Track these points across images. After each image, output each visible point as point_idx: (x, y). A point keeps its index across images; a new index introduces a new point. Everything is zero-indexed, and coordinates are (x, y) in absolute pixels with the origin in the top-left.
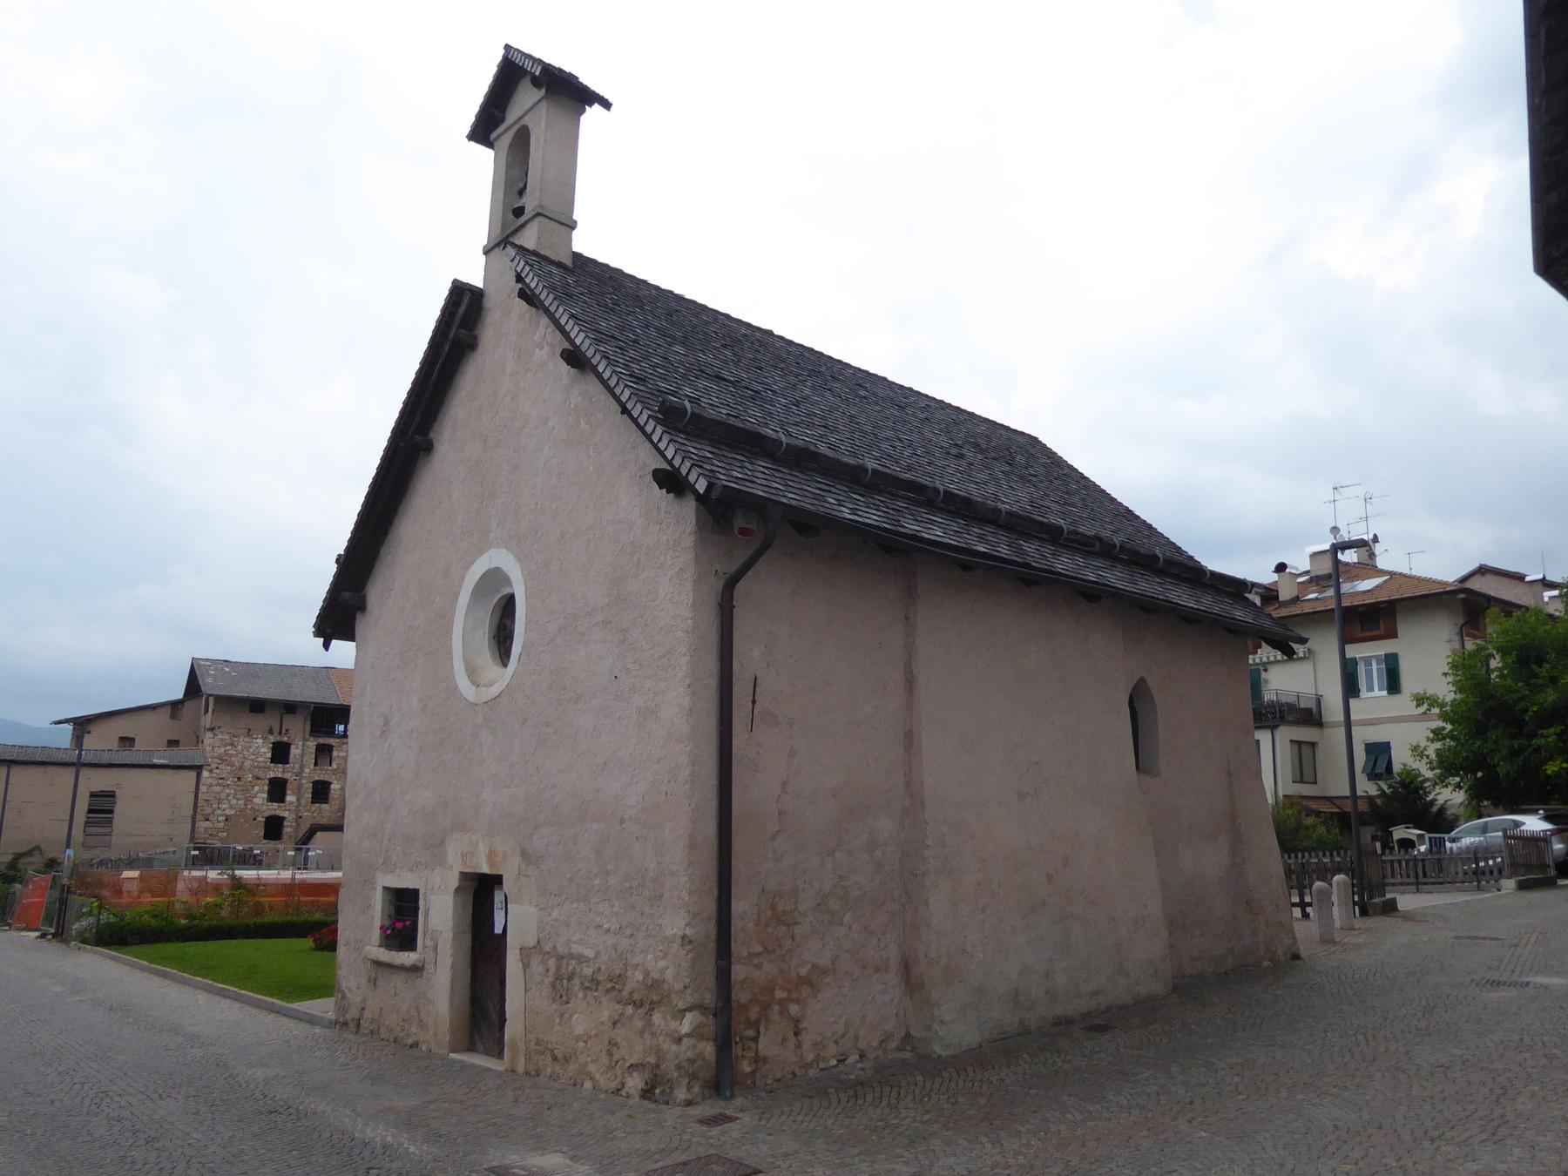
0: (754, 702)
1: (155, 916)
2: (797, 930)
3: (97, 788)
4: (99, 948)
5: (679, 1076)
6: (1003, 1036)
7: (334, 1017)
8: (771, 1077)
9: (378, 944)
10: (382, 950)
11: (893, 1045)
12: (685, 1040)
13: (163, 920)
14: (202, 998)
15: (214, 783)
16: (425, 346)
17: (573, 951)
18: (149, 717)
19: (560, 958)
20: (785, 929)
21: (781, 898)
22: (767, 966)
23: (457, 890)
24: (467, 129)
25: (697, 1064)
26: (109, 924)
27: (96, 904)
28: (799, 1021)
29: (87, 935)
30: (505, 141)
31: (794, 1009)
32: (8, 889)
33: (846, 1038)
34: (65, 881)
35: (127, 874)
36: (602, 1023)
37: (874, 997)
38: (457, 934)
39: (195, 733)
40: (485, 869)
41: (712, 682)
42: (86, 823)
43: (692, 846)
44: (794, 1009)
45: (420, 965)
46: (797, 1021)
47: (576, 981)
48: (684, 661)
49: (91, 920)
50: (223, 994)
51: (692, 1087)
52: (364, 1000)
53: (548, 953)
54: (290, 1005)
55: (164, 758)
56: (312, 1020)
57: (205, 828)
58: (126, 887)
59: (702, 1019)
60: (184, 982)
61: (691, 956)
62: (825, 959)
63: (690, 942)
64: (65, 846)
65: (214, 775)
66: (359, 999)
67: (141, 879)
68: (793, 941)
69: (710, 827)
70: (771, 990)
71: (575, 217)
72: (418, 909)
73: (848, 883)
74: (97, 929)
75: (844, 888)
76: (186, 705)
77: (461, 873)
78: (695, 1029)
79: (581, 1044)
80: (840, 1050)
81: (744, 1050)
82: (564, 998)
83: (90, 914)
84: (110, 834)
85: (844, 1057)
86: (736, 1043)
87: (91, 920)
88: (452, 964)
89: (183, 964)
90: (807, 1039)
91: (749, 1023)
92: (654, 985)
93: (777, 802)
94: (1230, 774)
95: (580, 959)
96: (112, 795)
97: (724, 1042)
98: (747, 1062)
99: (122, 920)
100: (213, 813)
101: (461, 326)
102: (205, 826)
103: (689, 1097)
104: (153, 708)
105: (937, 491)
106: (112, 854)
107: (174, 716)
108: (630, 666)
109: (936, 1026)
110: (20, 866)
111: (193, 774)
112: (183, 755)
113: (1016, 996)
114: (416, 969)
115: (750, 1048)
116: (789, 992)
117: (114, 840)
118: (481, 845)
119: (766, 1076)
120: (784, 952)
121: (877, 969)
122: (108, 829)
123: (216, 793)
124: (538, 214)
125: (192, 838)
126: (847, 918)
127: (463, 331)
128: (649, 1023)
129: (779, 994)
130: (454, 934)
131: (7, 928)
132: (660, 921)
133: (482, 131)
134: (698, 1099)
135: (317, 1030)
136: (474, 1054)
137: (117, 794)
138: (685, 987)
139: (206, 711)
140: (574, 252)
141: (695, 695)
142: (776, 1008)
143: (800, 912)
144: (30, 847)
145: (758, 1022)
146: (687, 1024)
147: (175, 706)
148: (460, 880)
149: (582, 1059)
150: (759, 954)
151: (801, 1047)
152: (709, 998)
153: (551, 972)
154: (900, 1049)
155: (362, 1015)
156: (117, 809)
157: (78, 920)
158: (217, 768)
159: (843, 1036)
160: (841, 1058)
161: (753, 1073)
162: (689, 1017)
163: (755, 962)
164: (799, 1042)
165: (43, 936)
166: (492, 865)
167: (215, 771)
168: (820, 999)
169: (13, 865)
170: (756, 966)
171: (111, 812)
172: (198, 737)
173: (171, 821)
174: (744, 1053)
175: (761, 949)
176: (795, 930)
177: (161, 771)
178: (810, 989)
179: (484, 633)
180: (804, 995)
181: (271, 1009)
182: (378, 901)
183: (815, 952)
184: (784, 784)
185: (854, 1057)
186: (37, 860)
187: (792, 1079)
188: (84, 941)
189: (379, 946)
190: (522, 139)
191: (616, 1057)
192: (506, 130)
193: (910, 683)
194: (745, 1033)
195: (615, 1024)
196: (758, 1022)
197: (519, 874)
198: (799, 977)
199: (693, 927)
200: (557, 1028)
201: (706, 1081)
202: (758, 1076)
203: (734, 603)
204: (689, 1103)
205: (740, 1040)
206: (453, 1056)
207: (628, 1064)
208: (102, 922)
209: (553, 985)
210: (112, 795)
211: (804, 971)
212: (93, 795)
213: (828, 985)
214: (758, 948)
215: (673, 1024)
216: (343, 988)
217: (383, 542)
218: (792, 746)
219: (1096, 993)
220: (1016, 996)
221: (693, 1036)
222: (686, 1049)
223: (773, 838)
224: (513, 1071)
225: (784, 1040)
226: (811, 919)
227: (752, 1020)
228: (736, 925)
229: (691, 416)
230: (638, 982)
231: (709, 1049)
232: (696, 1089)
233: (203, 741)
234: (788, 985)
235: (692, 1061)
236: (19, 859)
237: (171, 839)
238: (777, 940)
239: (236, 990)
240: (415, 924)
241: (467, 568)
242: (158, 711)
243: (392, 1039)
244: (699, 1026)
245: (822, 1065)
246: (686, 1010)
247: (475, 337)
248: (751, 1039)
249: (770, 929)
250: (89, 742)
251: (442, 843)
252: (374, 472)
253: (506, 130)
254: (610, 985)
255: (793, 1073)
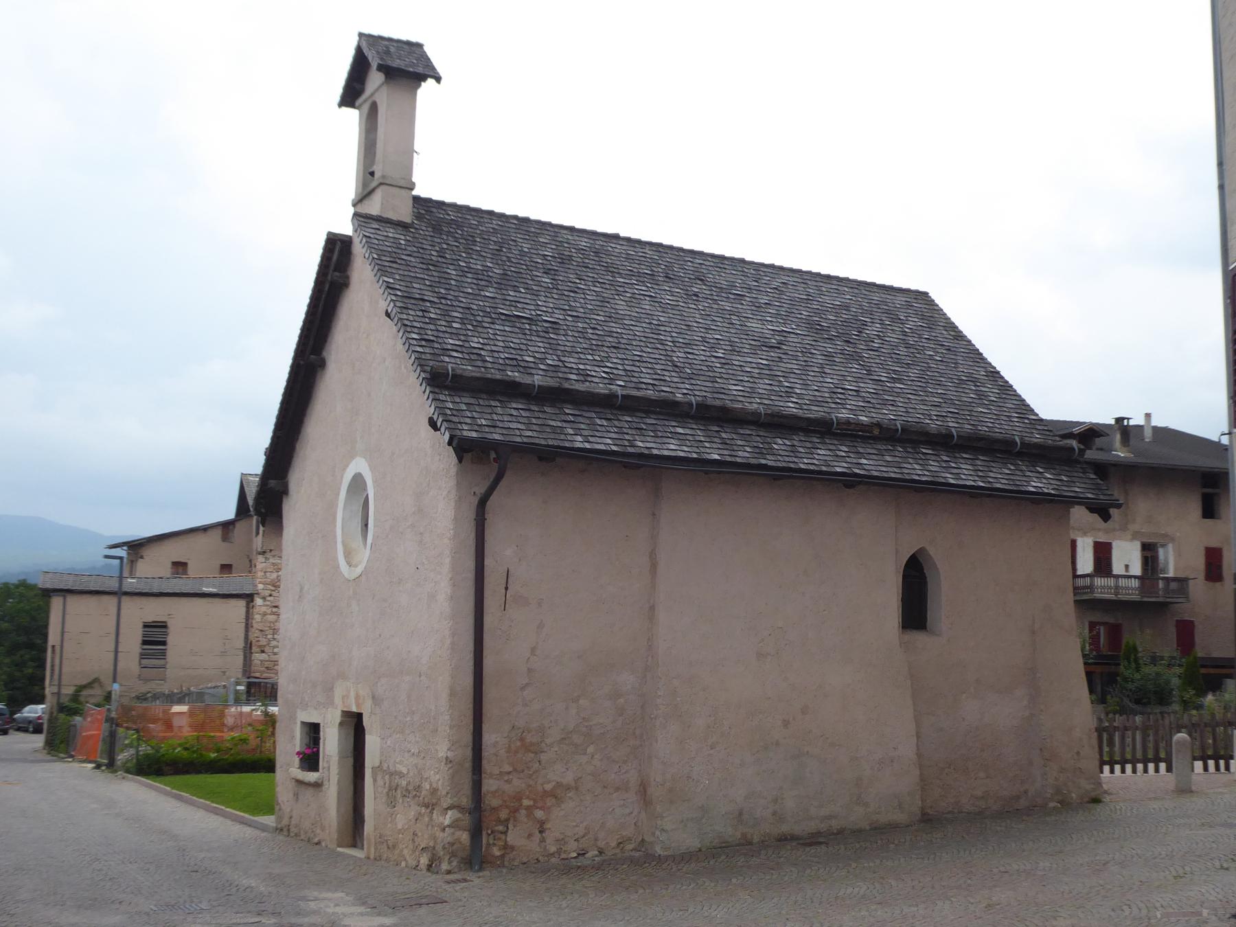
0: (506, 588)
1: (186, 749)
2: (543, 757)
3: (150, 618)
4: (139, 778)
5: (444, 855)
6: (724, 845)
7: (274, 825)
8: (518, 860)
9: (297, 767)
10: (299, 770)
11: (631, 847)
12: (447, 829)
13: (194, 752)
14: (200, 814)
15: (269, 611)
16: (312, 284)
17: (397, 769)
18: (201, 539)
19: (391, 774)
20: (532, 755)
21: (529, 732)
22: (516, 782)
23: (341, 724)
24: (338, 99)
25: (455, 847)
26: (147, 756)
27: (135, 736)
28: (544, 823)
29: (129, 765)
30: (366, 107)
31: (539, 814)
32: (70, 721)
33: (586, 838)
34: (113, 715)
35: (177, 709)
36: (410, 820)
37: (614, 809)
38: (342, 757)
39: (248, 556)
40: (354, 709)
41: (470, 575)
42: (141, 654)
43: (453, 694)
44: (539, 814)
45: (320, 781)
46: (542, 823)
47: (399, 792)
48: (448, 560)
49: (132, 751)
50: (216, 812)
51: (452, 862)
52: (291, 811)
53: (385, 771)
54: (256, 818)
55: (214, 586)
56: (263, 828)
57: (261, 661)
58: (176, 722)
59: (460, 815)
60: (192, 804)
61: (451, 771)
62: (569, 778)
63: (451, 761)
64: (111, 680)
65: (268, 603)
66: (288, 810)
67: (191, 713)
68: (540, 764)
69: (468, 681)
70: (520, 800)
71: (414, 180)
72: (320, 739)
73: (591, 723)
74: (138, 760)
75: (587, 727)
76: (238, 525)
77: (343, 711)
78: (453, 822)
79: (401, 836)
80: (581, 846)
81: (495, 840)
82: (393, 804)
83: (130, 746)
84: (164, 667)
85: (583, 852)
86: (489, 835)
87: (132, 751)
88: (338, 780)
89: (212, 795)
90: (550, 837)
91: (499, 821)
92: (434, 791)
93: (527, 662)
94: (1033, 632)
95: (401, 775)
96: (163, 626)
97: (476, 832)
98: (498, 848)
99: (158, 751)
100: (268, 644)
101: (335, 270)
102: (261, 658)
103: (449, 868)
104: (205, 529)
105: (690, 404)
106: (165, 688)
107: (225, 538)
108: (424, 561)
109: (658, 833)
110: (82, 699)
111: (242, 604)
112: (234, 583)
113: (741, 814)
114: (317, 785)
115: (500, 839)
116: (535, 801)
117: (169, 672)
118: (352, 690)
119: (514, 860)
120: (531, 773)
121: (617, 789)
122: (162, 662)
123: (271, 622)
124: (381, 184)
125: (81, 688)
126: (591, 749)
127: (337, 274)
128: (431, 819)
129: (526, 802)
130: (340, 757)
131: (70, 760)
132: (436, 747)
133: (350, 96)
134: (456, 870)
135: (264, 834)
136: (355, 849)
137: (169, 624)
138: (447, 793)
139: (258, 533)
140: (417, 199)
141: (454, 586)
142: (523, 812)
143: (546, 744)
144: (89, 680)
145: (507, 820)
146: (448, 819)
147: (226, 526)
148: (342, 716)
149: (401, 846)
150: (509, 773)
151: (545, 842)
152: (465, 801)
153: (387, 785)
154: (634, 849)
155: (290, 822)
156: (170, 640)
157: (122, 751)
158: (271, 595)
159: (584, 836)
160: (581, 852)
161: (503, 856)
162: (450, 813)
163: (506, 778)
164: (544, 838)
165: (98, 767)
166: (358, 705)
167: (269, 598)
168: (563, 807)
169: (75, 697)
170: (506, 781)
171: (164, 643)
172: (250, 561)
173: (223, 654)
174: (495, 842)
175: (511, 769)
176: (542, 757)
177: (210, 600)
178: (554, 800)
179: (358, 523)
180: (549, 804)
181: (243, 822)
182: (298, 731)
183: (557, 774)
184: (533, 650)
185: (592, 853)
186: (97, 692)
187: (535, 863)
188: (128, 771)
189: (299, 768)
190: (374, 109)
191: (417, 843)
192: (365, 101)
193: (654, 566)
194: (496, 828)
195: (416, 820)
196: (507, 820)
197: (371, 713)
198: (545, 791)
199: (452, 751)
200: (389, 825)
201: (462, 858)
202: (507, 859)
203: (486, 517)
204: (449, 872)
205: (492, 832)
206: (339, 849)
207: (421, 848)
208: (141, 753)
209: (388, 794)
210: (163, 626)
211: (548, 787)
212: (146, 626)
213: (570, 798)
214: (507, 768)
215: (441, 819)
216: (280, 802)
217: (298, 439)
218: (542, 620)
219: (830, 817)
220: (741, 814)
221: (452, 827)
222: (445, 837)
223: (523, 689)
224: (369, 858)
225: (530, 836)
226: (556, 749)
227: (502, 819)
228: (487, 753)
229: (452, 378)
230: (427, 790)
231: (465, 837)
232: (455, 864)
233: (255, 566)
234: (534, 797)
235: (452, 844)
236: (80, 691)
237: (224, 672)
238: (526, 764)
239: (223, 808)
240: (318, 751)
241: (344, 469)
242: (210, 533)
243: (306, 839)
244: (457, 820)
245: (563, 856)
246: (447, 809)
247: (348, 278)
248: (502, 833)
249: (519, 755)
250: (143, 568)
251: (332, 689)
252: (284, 384)
253: (365, 101)
254: (414, 793)
255: (537, 859)
